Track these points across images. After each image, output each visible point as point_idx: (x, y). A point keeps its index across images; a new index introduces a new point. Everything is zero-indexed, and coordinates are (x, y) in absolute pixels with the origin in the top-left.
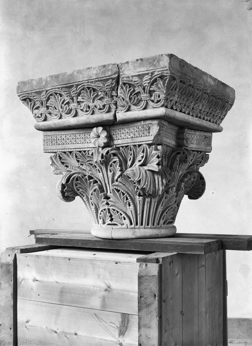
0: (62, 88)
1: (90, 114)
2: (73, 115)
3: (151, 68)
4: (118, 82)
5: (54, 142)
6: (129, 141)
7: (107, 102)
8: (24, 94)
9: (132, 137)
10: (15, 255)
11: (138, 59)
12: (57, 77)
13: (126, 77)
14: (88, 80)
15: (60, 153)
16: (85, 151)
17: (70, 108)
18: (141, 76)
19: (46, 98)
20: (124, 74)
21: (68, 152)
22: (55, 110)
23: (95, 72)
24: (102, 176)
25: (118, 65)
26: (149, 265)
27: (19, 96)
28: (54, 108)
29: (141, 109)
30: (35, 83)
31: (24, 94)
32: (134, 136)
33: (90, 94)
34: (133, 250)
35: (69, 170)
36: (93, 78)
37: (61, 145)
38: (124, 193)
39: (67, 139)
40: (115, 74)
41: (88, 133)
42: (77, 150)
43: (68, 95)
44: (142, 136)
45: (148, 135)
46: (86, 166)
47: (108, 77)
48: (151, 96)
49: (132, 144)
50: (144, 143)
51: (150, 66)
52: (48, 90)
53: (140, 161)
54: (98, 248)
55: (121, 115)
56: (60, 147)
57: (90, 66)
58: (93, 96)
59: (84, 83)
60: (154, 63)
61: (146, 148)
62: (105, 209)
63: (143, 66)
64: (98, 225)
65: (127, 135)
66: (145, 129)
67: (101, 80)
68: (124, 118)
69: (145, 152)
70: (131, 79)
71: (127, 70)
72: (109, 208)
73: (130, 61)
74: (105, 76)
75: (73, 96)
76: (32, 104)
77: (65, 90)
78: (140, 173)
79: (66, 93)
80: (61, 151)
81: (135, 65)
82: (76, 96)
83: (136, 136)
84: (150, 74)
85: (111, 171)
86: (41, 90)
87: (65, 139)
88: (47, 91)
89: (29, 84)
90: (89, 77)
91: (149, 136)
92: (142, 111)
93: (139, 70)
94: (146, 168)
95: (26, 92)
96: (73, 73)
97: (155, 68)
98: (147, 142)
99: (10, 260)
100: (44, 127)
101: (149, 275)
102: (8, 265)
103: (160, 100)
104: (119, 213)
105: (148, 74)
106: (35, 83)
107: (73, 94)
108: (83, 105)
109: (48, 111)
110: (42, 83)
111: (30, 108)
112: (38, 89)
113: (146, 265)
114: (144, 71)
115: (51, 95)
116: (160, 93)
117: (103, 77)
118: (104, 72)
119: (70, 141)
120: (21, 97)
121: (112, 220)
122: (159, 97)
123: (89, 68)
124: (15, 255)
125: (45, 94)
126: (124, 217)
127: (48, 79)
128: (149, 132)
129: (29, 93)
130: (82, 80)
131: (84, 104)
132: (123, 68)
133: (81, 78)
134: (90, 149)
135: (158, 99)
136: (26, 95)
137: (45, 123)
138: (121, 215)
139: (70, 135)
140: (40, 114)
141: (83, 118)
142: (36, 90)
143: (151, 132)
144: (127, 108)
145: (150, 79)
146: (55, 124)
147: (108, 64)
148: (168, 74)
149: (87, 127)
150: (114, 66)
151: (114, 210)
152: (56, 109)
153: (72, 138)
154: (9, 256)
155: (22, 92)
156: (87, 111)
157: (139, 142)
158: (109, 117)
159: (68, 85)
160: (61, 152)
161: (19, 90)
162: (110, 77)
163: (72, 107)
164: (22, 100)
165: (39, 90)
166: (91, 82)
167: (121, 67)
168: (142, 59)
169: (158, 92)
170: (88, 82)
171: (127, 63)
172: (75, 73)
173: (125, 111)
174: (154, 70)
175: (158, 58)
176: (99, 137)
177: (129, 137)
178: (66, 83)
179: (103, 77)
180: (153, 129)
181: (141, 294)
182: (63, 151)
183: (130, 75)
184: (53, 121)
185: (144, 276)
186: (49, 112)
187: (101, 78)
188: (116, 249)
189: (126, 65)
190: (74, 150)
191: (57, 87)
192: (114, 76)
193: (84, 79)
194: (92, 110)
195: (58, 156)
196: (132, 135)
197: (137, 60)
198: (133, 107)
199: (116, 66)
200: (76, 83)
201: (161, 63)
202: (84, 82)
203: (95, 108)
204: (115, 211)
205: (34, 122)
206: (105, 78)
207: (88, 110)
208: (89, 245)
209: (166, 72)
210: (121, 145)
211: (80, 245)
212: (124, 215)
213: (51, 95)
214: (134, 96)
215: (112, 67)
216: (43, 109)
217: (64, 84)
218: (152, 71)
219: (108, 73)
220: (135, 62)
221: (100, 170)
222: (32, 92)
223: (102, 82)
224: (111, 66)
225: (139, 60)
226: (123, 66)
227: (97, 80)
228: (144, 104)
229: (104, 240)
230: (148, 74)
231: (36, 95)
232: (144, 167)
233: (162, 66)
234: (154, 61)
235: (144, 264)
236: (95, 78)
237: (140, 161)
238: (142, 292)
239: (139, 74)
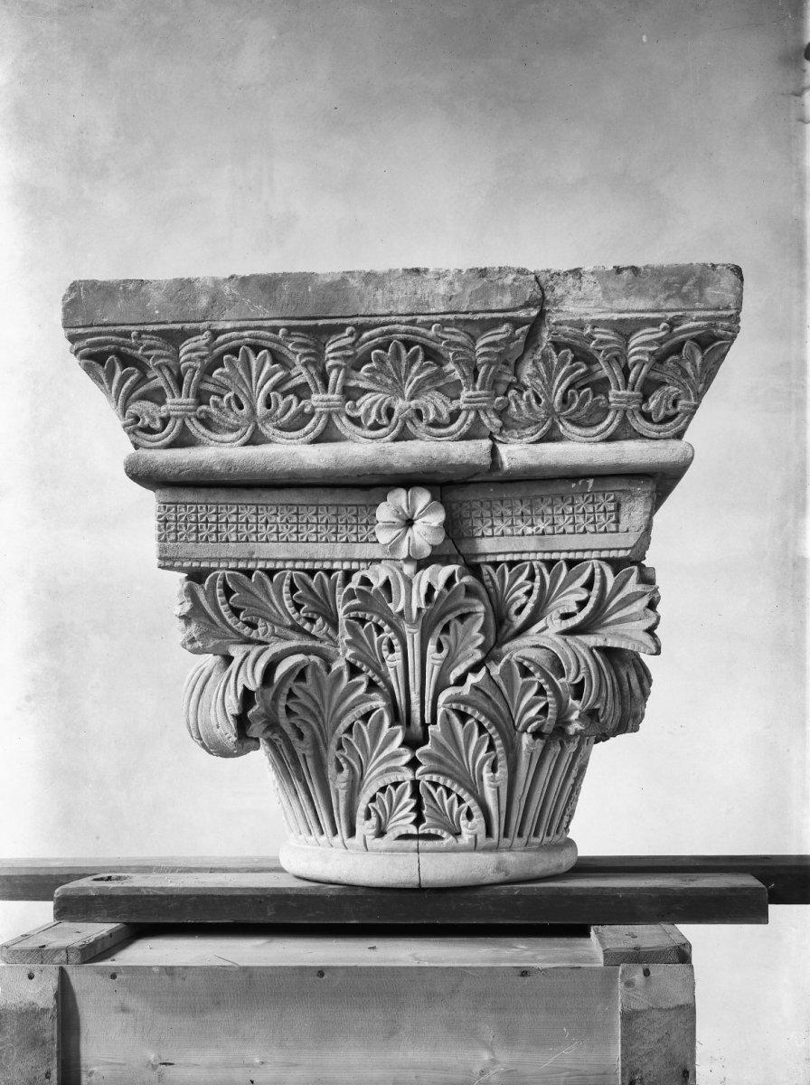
0: (290, 329)
1: (388, 438)
2: (311, 435)
3: (669, 305)
4: (532, 339)
5: (205, 532)
6: (531, 544)
7: (470, 402)
8: (99, 334)
9: (540, 531)
10: (62, 971)
11: (622, 264)
12: (268, 285)
13: (571, 323)
14: (413, 315)
15: (227, 572)
16: (329, 572)
17: (307, 410)
18: (625, 329)
19: (206, 361)
20: (558, 311)
21: (260, 569)
22: (236, 409)
23: (442, 289)
24: (399, 663)
25: (537, 279)
26: (658, 970)
27: (72, 339)
28: (233, 403)
29: (598, 438)
30: (157, 297)
31: (99, 334)
32: (550, 530)
33: (409, 367)
34: (501, 922)
35: (261, 638)
36: (433, 310)
37: (233, 545)
38: (486, 725)
39: (264, 521)
40: (527, 305)
41: (349, 505)
42: (298, 565)
43: (312, 359)
44: (585, 531)
45: (613, 528)
46: (269, 628)
47: (501, 315)
48: (645, 399)
49: (539, 556)
50: (595, 554)
51: (669, 297)
52: (223, 332)
53: (565, 616)
54: (354, 922)
55: (517, 453)
56: (233, 550)
57: (421, 266)
58: (418, 373)
59: (394, 323)
60: (685, 289)
61: (602, 572)
62: (396, 785)
63: (641, 293)
64: (349, 841)
65: (581, 520)
66: (602, 509)
67: (468, 321)
68: (532, 462)
69: (597, 585)
70: (588, 330)
71: (574, 300)
72: (417, 778)
73: (588, 268)
74: (488, 308)
75: (183, 366)
76: (132, 378)
77: (300, 340)
78: (578, 661)
79: (302, 351)
80: (232, 565)
81: (611, 285)
82: (345, 367)
83: (561, 530)
84: (663, 325)
85: (440, 648)
86: (187, 326)
87: (254, 520)
88: (215, 334)
89: (127, 299)
90: (418, 304)
91: (617, 532)
92: (602, 446)
93: (624, 303)
94: (592, 640)
95: (112, 329)
96: (344, 280)
97: (688, 307)
98: (604, 554)
99: (41, 992)
100: (176, 471)
101: (664, 1005)
102: (30, 1014)
103: (675, 415)
104: (454, 796)
105: (654, 323)
106: (157, 297)
107: (334, 358)
108: (366, 401)
109: (201, 412)
110: (194, 300)
111: (118, 391)
112: (173, 322)
113: (647, 973)
114: (642, 311)
115: (234, 351)
116: (681, 391)
117: (476, 312)
118: (483, 293)
119: (274, 530)
120: (81, 344)
121: (418, 821)
122: (675, 404)
123: (417, 271)
124: (62, 971)
125: (207, 345)
126: (469, 809)
127: (227, 289)
128: (617, 521)
129: (127, 335)
130: (387, 311)
131: (373, 398)
132: (559, 291)
133: (391, 303)
134: (355, 566)
135: (672, 412)
136: (114, 338)
137: (184, 456)
138: (461, 801)
139: (355, 508)
140: (162, 419)
141: (359, 450)
142: (164, 323)
143: (624, 518)
144: (544, 428)
145: (660, 341)
146: (230, 462)
147: (500, 268)
148: (730, 331)
149: (370, 485)
150: (522, 277)
151: (436, 785)
152: (241, 407)
153: (284, 521)
154: (31, 977)
155: (91, 326)
156: (375, 427)
157: (569, 551)
158: (473, 455)
159: (321, 322)
160: (299, 570)
161: (75, 314)
162: (509, 314)
163: (315, 404)
164: (82, 357)
165: (178, 326)
166: (423, 324)
167: (551, 283)
168: (634, 269)
169: (676, 389)
170: (413, 323)
171: (577, 273)
172: (353, 282)
173: (532, 439)
174: (680, 313)
175: (698, 274)
176: (409, 523)
177: (529, 530)
178: (309, 312)
179: (476, 312)
180: (631, 509)
181: (634, 1073)
182: (241, 565)
183: (585, 318)
184: (219, 452)
185: (643, 1011)
186: (203, 415)
187: (467, 313)
188: (431, 922)
189: (570, 280)
190: (289, 565)
191: (267, 324)
192: (522, 314)
193: (392, 308)
194: (400, 423)
195: (219, 583)
196: (542, 526)
197: (618, 270)
198: (565, 428)
199: (532, 277)
200: (360, 320)
201: (709, 290)
202: (393, 318)
203: (416, 421)
204: (440, 789)
205: (123, 447)
206: (489, 316)
207: (385, 421)
208: (312, 915)
209: (726, 324)
210: (490, 559)
211: (270, 916)
212: (470, 802)
213: (234, 351)
214: (586, 390)
215: (515, 280)
216: (177, 400)
217: (303, 315)
218: (674, 314)
219: (502, 301)
220: (608, 273)
221: (395, 642)
222: (146, 332)
223: (469, 329)
224: (511, 277)
225: (626, 269)
226: (556, 284)
227: (451, 317)
228: (612, 422)
229: (379, 893)
230: (654, 323)
231: (158, 344)
232: (579, 637)
233: (713, 302)
234: (684, 283)
235: (639, 969)
236: (442, 309)
237: (565, 616)
238: (638, 1065)
239: (625, 320)
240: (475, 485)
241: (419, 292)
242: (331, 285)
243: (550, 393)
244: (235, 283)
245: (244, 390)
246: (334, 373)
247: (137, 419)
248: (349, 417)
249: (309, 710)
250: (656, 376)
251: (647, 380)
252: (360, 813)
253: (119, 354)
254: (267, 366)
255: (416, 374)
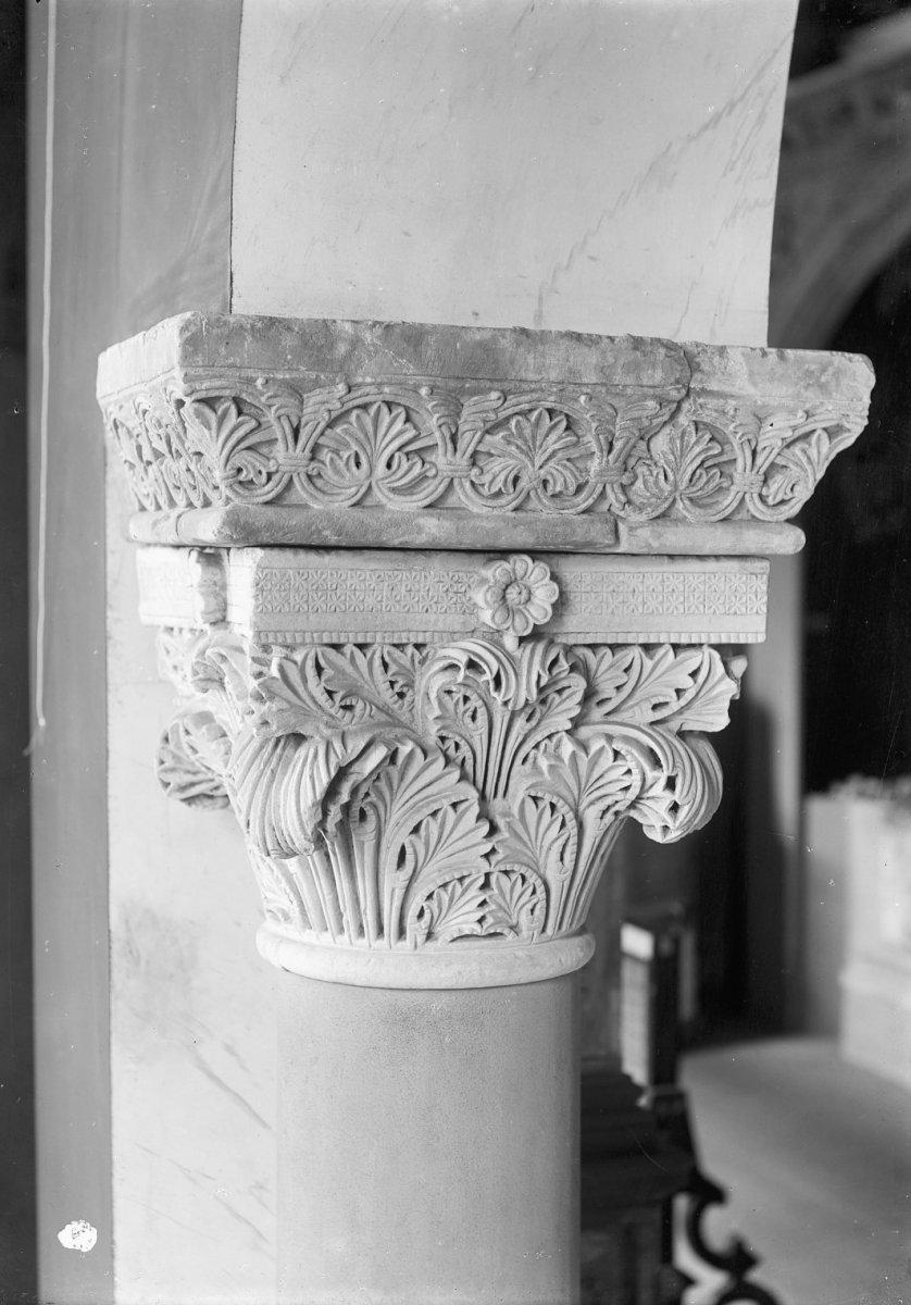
22: (354, 468)
96: (494, 339)
108: (495, 466)
110: (332, 346)
127: (368, 337)
161: (195, 352)
240: (585, 556)
241: (571, 359)
242: (481, 344)
243: (678, 470)
244: (378, 331)
245: (368, 448)
246: (468, 435)
247: (239, 470)
248: (472, 483)
249: (312, 777)
250: (780, 461)
251: (773, 465)
252: (412, 912)
253: (237, 401)
254: (399, 425)
255: (553, 442)
